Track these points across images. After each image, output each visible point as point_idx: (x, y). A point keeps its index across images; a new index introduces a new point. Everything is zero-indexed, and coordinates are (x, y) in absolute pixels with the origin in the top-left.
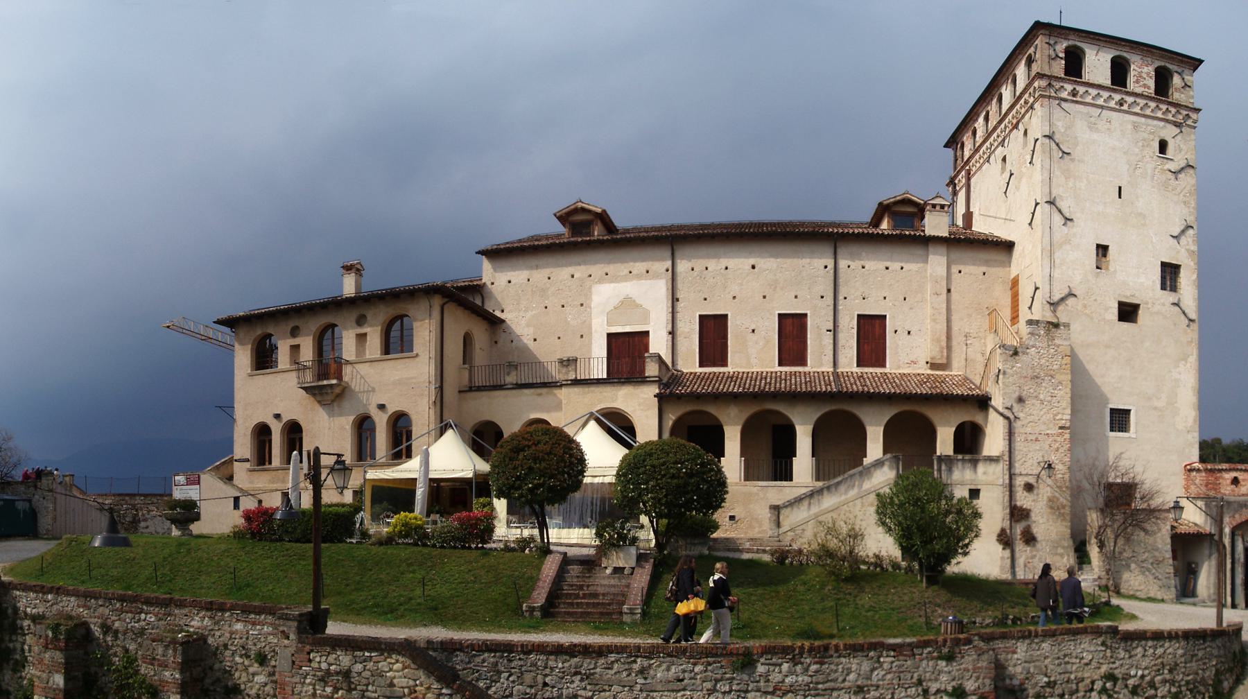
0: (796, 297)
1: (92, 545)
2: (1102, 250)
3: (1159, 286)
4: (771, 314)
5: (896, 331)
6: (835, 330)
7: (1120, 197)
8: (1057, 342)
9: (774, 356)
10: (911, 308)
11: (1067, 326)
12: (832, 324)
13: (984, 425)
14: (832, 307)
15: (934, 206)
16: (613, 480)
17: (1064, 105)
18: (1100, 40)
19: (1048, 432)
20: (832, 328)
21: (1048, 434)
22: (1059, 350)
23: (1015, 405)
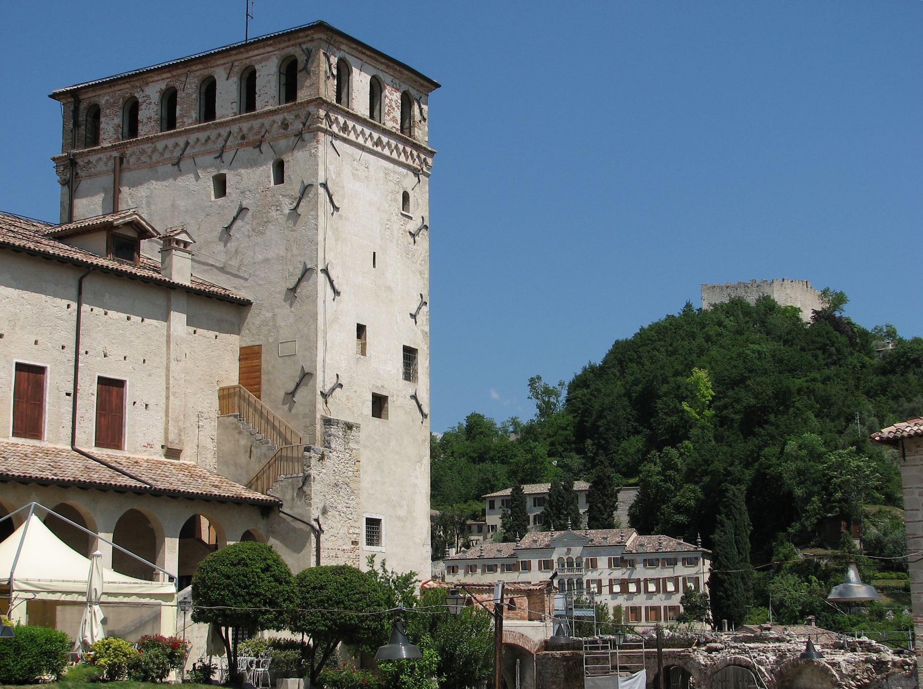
0: (36, 343)
1: (854, 566)
2: (361, 330)
3: (401, 376)
4: (8, 362)
5: (134, 403)
6: (74, 395)
7: (374, 266)
8: (352, 445)
9: (9, 423)
10: (150, 375)
11: (358, 427)
12: (72, 386)
13: (15, 526)
14: (73, 363)
15: (178, 242)
16: (295, 572)
17: (337, 143)
18: (364, 53)
19: (344, 547)
20: (72, 391)
21: (344, 550)
22: (353, 455)
23: (320, 516)
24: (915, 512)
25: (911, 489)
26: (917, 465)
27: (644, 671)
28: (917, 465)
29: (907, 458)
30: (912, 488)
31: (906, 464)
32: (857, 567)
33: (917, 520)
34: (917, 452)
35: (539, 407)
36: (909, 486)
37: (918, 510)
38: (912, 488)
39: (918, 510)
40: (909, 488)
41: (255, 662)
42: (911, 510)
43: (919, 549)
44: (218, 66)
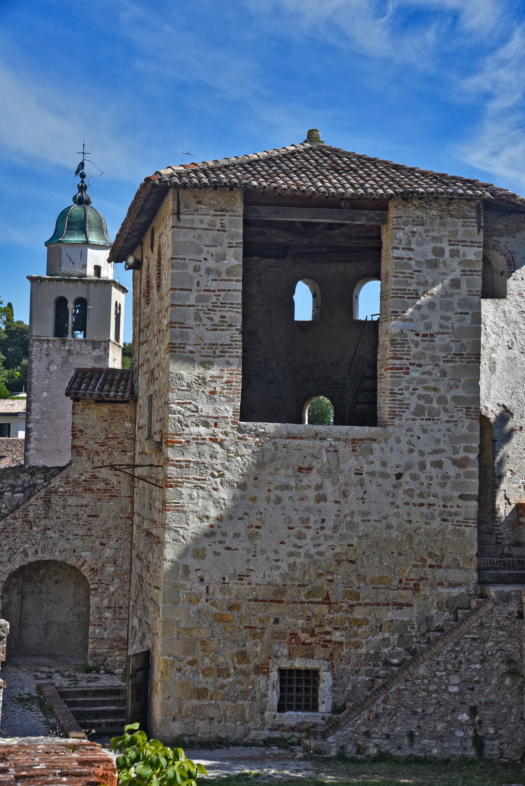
24: (186, 293)
25: (184, 261)
26: (194, 229)
27: (109, 251)
28: (194, 229)
29: (182, 217)
30: (185, 259)
31: (180, 225)
32: (477, 399)
33: (187, 303)
34: (197, 210)
35: (301, 657)
36: (182, 256)
37: (191, 290)
38: (185, 259)
39: (191, 290)
40: (182, 259)
41: (443, 313)
42: (180, 289)
43: (185, 344)
44: (19, 398)
